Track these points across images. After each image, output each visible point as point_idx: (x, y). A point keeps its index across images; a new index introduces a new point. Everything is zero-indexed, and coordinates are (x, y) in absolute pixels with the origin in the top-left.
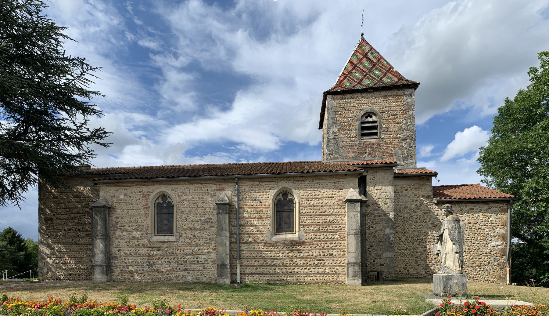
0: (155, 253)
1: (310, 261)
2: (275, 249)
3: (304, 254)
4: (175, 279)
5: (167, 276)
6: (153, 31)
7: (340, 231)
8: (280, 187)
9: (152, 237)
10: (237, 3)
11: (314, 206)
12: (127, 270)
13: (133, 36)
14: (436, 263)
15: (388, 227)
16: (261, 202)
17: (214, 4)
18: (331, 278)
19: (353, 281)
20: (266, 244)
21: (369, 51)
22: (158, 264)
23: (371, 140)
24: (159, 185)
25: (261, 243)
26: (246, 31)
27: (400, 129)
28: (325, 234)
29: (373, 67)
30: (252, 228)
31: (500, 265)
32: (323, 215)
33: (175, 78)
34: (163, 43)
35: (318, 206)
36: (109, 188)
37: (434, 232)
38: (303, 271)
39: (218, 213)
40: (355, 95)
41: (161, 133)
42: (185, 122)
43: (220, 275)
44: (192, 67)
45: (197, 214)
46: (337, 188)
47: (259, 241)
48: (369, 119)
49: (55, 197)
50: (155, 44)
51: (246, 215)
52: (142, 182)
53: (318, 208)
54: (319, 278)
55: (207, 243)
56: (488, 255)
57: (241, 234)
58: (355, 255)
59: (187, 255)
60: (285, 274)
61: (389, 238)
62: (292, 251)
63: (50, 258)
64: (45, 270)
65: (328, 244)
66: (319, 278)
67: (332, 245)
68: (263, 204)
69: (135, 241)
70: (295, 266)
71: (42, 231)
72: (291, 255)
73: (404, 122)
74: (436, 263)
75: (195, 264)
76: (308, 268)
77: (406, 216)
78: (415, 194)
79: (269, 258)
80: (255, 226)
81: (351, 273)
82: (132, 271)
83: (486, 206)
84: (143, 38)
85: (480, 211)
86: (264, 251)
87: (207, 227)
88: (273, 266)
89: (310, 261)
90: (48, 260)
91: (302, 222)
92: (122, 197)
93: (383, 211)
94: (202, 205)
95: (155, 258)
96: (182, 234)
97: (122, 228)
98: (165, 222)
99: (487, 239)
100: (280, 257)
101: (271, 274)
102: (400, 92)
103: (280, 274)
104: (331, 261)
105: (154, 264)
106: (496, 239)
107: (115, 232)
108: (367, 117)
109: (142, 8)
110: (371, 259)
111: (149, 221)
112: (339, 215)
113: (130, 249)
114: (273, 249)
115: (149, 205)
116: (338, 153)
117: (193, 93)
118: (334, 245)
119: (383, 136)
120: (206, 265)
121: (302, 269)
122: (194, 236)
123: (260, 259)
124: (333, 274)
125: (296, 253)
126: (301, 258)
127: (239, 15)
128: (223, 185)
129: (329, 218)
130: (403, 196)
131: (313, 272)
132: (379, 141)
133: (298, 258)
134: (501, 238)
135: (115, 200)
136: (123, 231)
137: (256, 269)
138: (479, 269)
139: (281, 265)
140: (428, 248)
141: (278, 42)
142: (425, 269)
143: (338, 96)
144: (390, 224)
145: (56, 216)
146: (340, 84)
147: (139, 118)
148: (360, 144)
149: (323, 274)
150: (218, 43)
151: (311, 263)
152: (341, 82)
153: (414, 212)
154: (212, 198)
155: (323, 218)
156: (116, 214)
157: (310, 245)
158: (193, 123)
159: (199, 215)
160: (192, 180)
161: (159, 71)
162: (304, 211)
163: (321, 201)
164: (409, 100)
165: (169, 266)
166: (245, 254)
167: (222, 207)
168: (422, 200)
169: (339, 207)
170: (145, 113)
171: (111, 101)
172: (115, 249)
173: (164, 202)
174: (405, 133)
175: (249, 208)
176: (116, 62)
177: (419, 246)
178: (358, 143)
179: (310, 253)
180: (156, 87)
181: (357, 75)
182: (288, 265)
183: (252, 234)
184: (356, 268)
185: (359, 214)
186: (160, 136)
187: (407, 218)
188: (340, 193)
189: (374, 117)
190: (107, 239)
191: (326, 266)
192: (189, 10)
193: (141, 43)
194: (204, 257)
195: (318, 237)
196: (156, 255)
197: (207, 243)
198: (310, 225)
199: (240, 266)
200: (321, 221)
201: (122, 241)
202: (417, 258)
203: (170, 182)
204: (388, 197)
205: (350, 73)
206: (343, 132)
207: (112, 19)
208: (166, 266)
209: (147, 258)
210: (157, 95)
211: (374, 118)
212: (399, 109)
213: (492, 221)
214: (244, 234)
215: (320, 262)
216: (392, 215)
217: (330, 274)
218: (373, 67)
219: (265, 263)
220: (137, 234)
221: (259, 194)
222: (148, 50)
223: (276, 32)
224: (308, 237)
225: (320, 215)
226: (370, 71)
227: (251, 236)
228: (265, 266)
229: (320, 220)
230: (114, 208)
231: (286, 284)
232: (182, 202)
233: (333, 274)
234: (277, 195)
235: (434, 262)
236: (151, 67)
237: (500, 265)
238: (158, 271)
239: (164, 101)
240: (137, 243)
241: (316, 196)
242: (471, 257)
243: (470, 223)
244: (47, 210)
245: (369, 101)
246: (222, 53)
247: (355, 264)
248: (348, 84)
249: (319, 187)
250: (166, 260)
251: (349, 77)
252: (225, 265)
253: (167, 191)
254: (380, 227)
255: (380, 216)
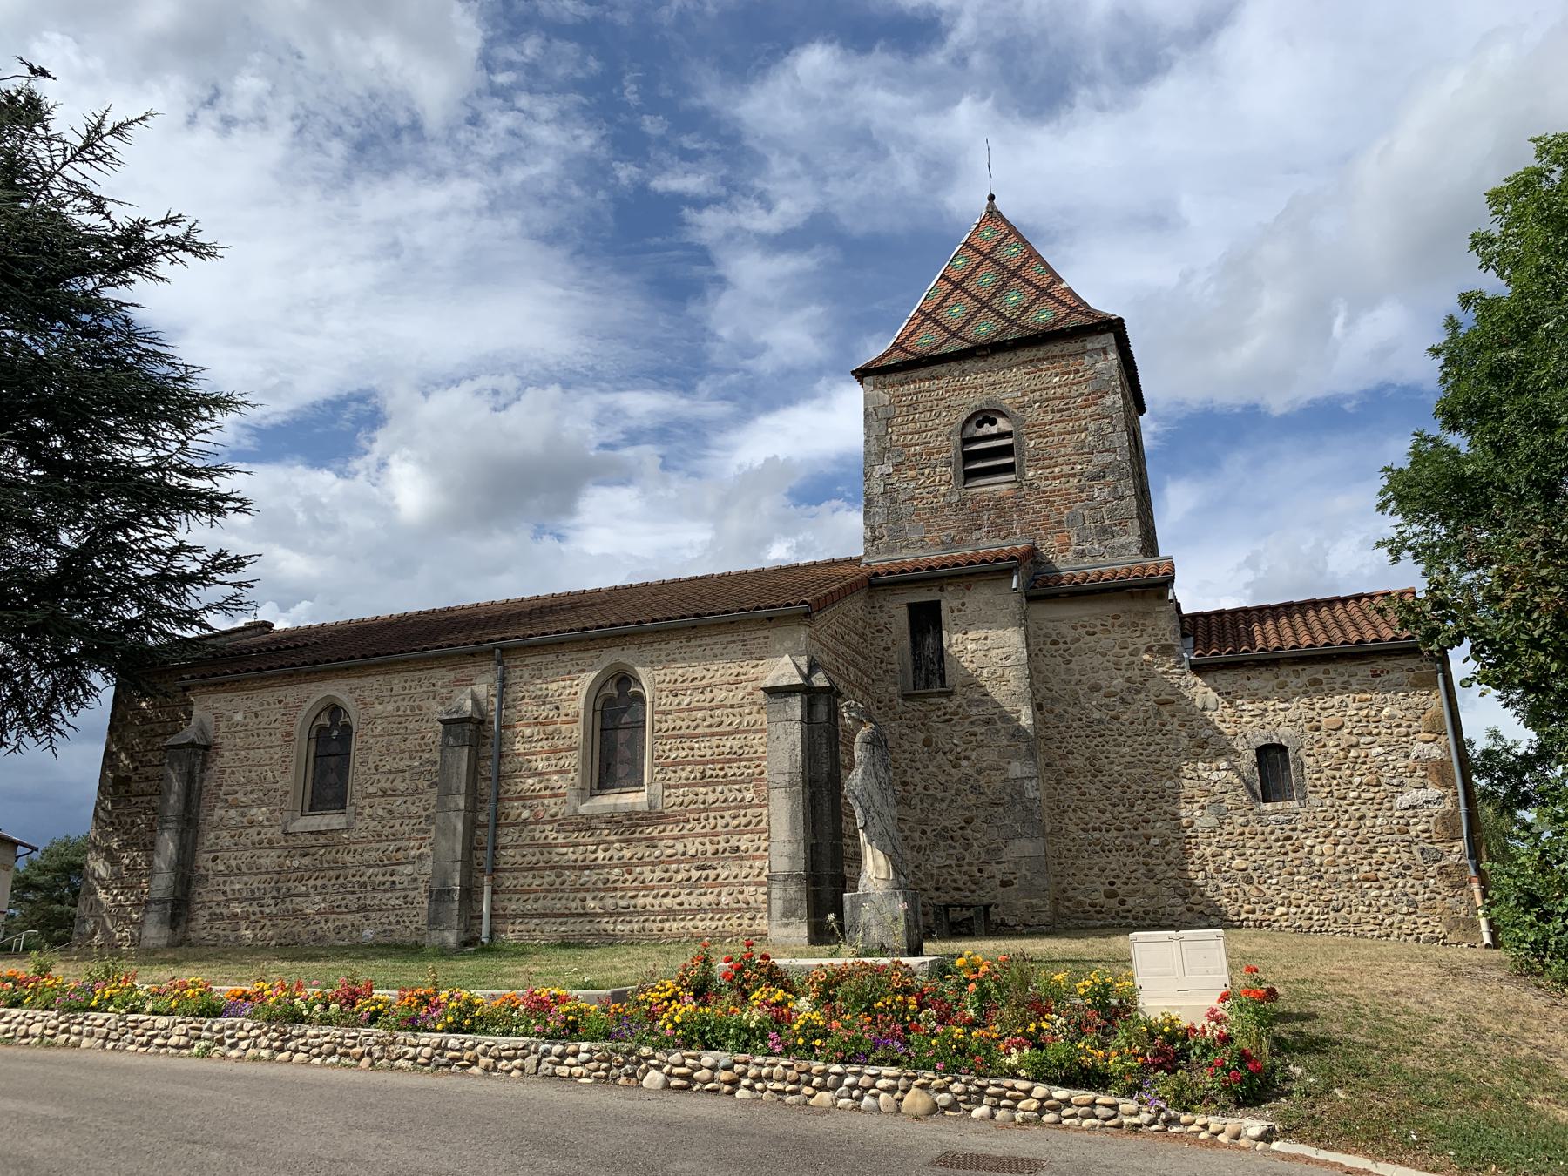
0: (296, 863)
1: (677, 871)
2: (587, 839)
3: (664, 849)
4: (332, 935)
5: (316, 927)
6: (696, 146)
7: (756, 778)
8: (606, 664)
9: (293, 820)
10: (949, 30)
11: (690, 710)
12: (225, 911)
13: (635, 169)
14: (1218, 871)
15: (1017, 756)
16: (557, 708)
17: (877, 48)
18: (735, 921)
19: (785, 931)
20: (562, 824)
21: (1002, 240)
22: (298, 895)
23: (999, 487)
24: (324, 679)
25: (550, 822)
26: (984, 98)
27: (1079, 450)
28: (719, 789)
29: (1005, 284)
30: (530, 781)
31: (1449, 875)
32: (713, 735)
33: (752, 271)
34: (724, 172)
35: (700, 709)
36: (213, 697)
37: (1200, 765)
38: (657, 902)
39: (445, 746)
40: (942, 369)
41: (707, 447)
42: (789, 401)
43: (434, 921)
44: (813, 233)
45: (403, 751)
46: (749, 655)
47: (547, 818)
48: (988, 429)
49: (146, 720)
50: (702, 178)
51: (519, 747)
52: (284, 676)
53: (700, 714)
54: (700, 924)
55: (418, 831)
56: (1398, 837)
57: (504, 800)
58: (788, 849)
59: (369, 866)
60: (611, 915)
61: (1021, 793)
62: (629, 842)
63: (107, 889)
64: (89, 928)
65: (727, 818)
66: (700, 924)
67: (736, 822)
68: (562, 711)
69: (253, 831)
70: (636, 889)
71: (101, 814)
72: (627, 853)
73: (1092, 426)
74: (1218, 871)
75: (385, 891)
76: (672, 892)
77: (1097, 715)
78: (1108, 649)
79: (569, 868)
80: (541, 774)
81: (777, 905)
82: (236, 915)
83: (1364, 670)
84: (665, 169)
85: (1345, 688)
86: (556, 846)
87: (423, 784)
88: (578, 890)
89: (677, 871)
90: (102, 895)
91: (659, 757)
92: (238, 717)
93: (997, 705)
94: (417, 726)
95: (294, 876)
96: (363, 808)
97: (230, 798)
98: (332, 777)
99: (1383, 781)
100: (599, 861)
101: (571, 915)
102: (1072, 347)
103: (596, 915)
104: (735, 870)
105: (289, 894)
106: (1417, 781)
107: (212, 809)
108: (980, 425)
109: (666, 91)
110: (970, 864)
111: (290, 778)
112: (756, 732)
113: (239, 854)
114: (580, 840)
115: (296, 734)
116: (897, 533)
117: (814, 310)
118: (744, 821)
119: (1031, 474)
120: (412, 894)
121: (655, 897)
122: (390, 812)
123: (545, 869)
124: (739, 910)
125: (641, 850)
126: (653, 864)
127: (961, 60)
128: (470, 671)
129: (732, 743)
130: (1081, 652)
131: (686, 906)
132: (1021, 488)
133: (646, 864)
134: (1435, 777)
135: (222, 725)
136: (231, 806)
137: (536, 901)
138: (1374, 893)
139: (600, 885)
140: (1184, 822)
141: (1100, 108)
142: (1185, 896)
143: (894, 378)
144: (1023, 747)
145: (141, 770)
146: (903, 342)
147: (643, 404)
148: (962, 502)
149: (713, 911)
150: (893, 149)
151: (679, 877)
152: (907, 338)
153: (1123, 701)
154: (443, 704)
155: (715, 741)
156: (220, 762)
157: (677, 823)
158: (816, 402)
159: (406, 755)
160: (396, 663)
161: (703, 255)
162: (664, 726)
163: (708, 696)
164: (1099, 366)
165: (324, 900)
166: (509, 856)
167: (457, 729)
168: (1147, 663)
169: (755, 708)
170: (663, 387)
171: (558, 364)
172: (206, 856)
173: (334, 724)
174: (1097, 459)
175: (528, 725)
176: (581, 251)
177: (1152, 817)
178: (955, 498)
179: (680, 848)
180: (693, 309)
181: (954, 313)
182: (619, 884)
183: (531, 798)
184: (793, 890)
185: (798, 726)
186: (704, 457)
187: (1100, 721)
188: (760, 669)
189: (1000, 420)
190: (190, 827)
191: (722, 885)
192: (796, 78)
193: (660, 184)
194: (409, 869)
195: (701, 798)
196: (297, 870)
197: (418, 831)
198: (679, 764)
199: (494, 892)
200: (710, 752)
201: (225, 833)
202: (1150, 855)
203: (347, 671)
204: (1009, 662)
205: (939, 307)
206: (911, 474)
207: (576, 138)
208: (318, 899)
209: (276, 877)
210: (701, 333)
211: (1002, 425)
212: (1073, 393)
213: (1390, 717)
214: (510, 799)
215: (704, 873)
216: (1026, 718)
217: (732, 910)
218: (1005, 284)
219: (558, 881)
220: (259, 814)
221: (554, 686)
222: (681, 199)
223: (1091, 80)
224: (672, 800)
225: (705, 735)
226: (994, 295)
227: (528, 803)
228: (557, 890)
229: (705, 748)
230: (217, 747)
231: (611, 941)
232: (371, 722)
233: (739, 910)
234: (597, 689)
235: (1210, 868)
236: (688, 246)
237: (1449, 875)
238: (297, 914)
239: (719, 347)
240: (256, 838)
241: (696, 683)
242: (1340, 848)
243: (1318, 729)
244: (123, 756)
245: (982, 379)
246: (908, 176)
247: (788, 877)
248: (926, 341)
249: (704, 657)
250: (319, 883)
251: (933, 320)
252: (449, 891)
253: (338, 695)
254: (989, 756)
255: (987, 722)
